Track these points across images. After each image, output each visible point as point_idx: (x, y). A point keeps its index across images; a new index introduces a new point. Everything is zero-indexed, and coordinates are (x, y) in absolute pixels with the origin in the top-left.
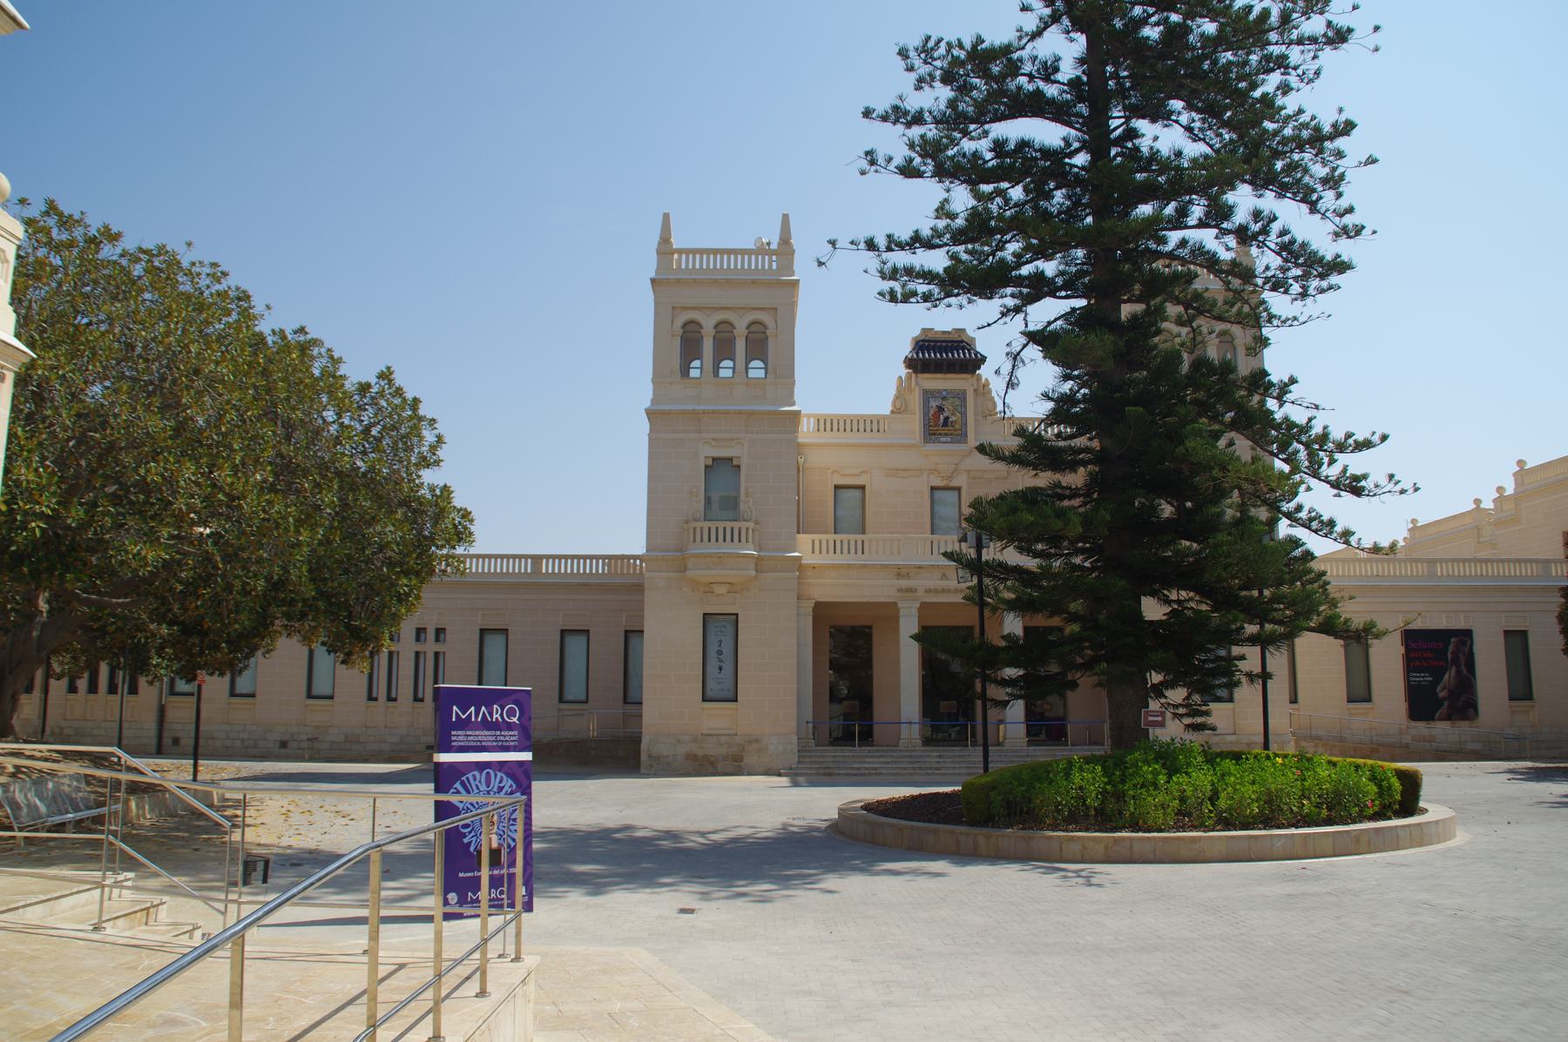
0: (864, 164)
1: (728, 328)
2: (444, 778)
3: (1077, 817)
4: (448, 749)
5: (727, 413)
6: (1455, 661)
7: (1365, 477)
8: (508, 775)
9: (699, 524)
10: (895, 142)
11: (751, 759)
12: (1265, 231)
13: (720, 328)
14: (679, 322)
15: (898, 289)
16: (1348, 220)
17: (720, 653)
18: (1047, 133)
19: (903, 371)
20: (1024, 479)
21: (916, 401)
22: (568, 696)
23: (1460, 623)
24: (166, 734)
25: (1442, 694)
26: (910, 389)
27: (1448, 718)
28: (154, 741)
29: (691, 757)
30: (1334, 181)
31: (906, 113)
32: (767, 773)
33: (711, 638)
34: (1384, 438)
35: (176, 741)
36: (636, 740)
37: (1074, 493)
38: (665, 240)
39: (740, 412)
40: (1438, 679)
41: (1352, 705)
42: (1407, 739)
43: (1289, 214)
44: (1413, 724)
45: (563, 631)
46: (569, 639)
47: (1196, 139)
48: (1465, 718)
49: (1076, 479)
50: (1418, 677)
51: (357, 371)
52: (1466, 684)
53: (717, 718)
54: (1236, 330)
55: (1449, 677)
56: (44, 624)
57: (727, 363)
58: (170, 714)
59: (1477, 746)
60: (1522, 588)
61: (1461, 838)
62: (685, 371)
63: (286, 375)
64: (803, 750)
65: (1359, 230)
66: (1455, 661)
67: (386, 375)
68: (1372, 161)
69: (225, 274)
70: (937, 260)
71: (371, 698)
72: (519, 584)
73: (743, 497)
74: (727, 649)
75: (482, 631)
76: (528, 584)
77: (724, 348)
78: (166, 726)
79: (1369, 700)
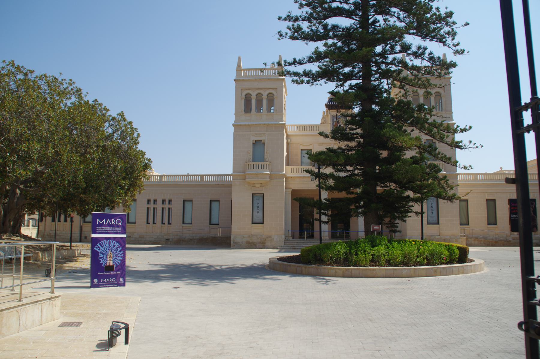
0: (278, 36)
1: (417, 94)
2: (94, 242)
3: (337, 262)
4: (95, 232)
5: (260, 125)
7: (461, 142)
8: (117, 242)
10: (284, 26)
11: (267, 244)
12: (423, 53)
14: (244, 94)
15: (299, 81)
16: (458, 48)
17: (258, 207)
18: (344, 22)
19: (325, 109)
20: (334, 144)
21: (329, 120)
22: (213, 222)
24: (83, 236)
26: (327, 115)
28: (79, 238)
29: (248, 243)
30: (453, 34)
31: (292, 17)
32: (274, 248)
33: (255, 202)
34: (470, 128)
35: (86, 238)
36: (229, 238)
37: (352, 149)
38: (239, 66)
39: (264, 124)
42: (510, 238)
43: (435, 48)
44: (512, 233)
45: (184, 201)
47: (401, 21)
49: (353, 144)
50: (514, 216)
51: (113, 113)
53: (257, 229)
54: (419, 89)
56: (18, 197)
58: (84, 229)
61: (486, 270)
63: (89, 115)
64: (286, 240)
65: (463, 51)
67: (122, 114)
68: (467, 24)
69: (74, 83)
70: (314, 67)
71: (148, 223)
72: (196, 185)
73: (265, 154)
75: (184, 201)
78: (83, 233)
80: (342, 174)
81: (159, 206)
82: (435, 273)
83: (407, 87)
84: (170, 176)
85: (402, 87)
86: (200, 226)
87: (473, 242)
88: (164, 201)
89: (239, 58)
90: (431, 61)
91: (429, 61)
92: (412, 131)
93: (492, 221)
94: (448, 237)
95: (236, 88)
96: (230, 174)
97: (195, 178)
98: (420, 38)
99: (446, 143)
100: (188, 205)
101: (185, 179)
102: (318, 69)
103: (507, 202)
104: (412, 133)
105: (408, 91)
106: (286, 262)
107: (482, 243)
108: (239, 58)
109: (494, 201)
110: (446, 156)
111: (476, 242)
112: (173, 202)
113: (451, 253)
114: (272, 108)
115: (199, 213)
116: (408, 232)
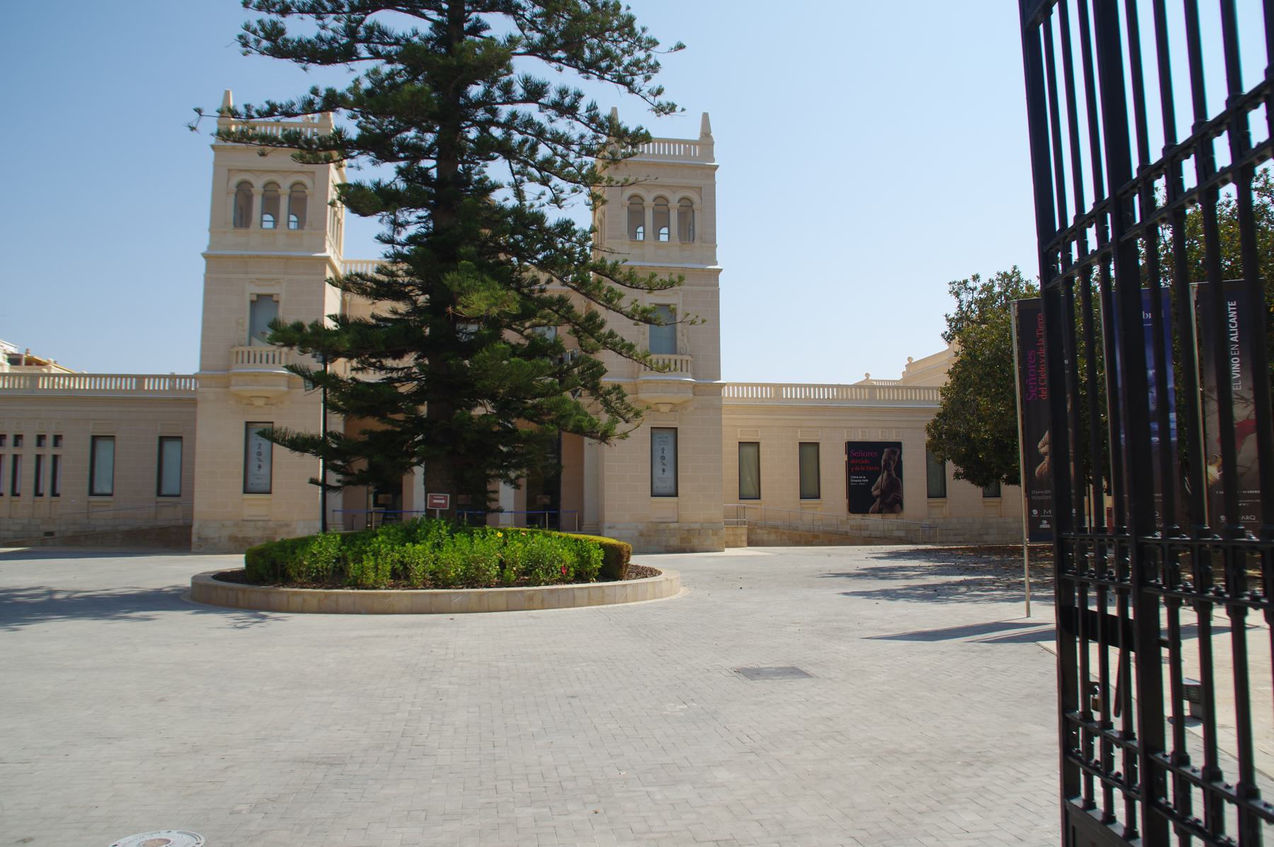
1: (664, 202)
3: (318, 580)
5: (269, 257)
9: (242, 349)
13: (295, 188)
17: (259, 454)
23: (892, 437)
27: (880, 511)
33: (656, 446)
39: (280, 257)
40: (873, 480)
41: (931, 500)
42: (847, 528)
43: (601, 94)
44: (853, 516)
45: (162, 439)
46: (100, 444)
48: (892, 512)
50: (856, 479)
55: (882, 479)
59: (902, 534)
62: (633, 234)
65: (672, 108)
68: (680, 47)
74: (669, 454)
76: (132, 399)
77: (662, 219)
79: (819, 497)
80: (372, 377)
81: (29, 451)
82: (528, 604)
83: (555, 181)
84: (101, 376)
85: (545, 182)
86: (132, 497)
87: (765, 537)
88: (40, 439)
89: (705, 116)
90: (593, 126)
91: (587, 125)
92: (549, 281)
93: (810, 490)
94: (697, 526)
95: (216, 166)
96: (191, 373)
97: (758, 393)
98: (576, 71)
100: (104, 449)
101: (86, 385)
102: (358, 131)
104: (548, 287)
105: (562, 192)
106: (237, 582)
107: (785, 537)
108: (705, 116)
109: (817, 444)
110: (623, 340)
111: (773, 537)
112: (64, 442)
113: (582, 557)
114: (640, 229)
115: (130, 465)
116: (606, 513)
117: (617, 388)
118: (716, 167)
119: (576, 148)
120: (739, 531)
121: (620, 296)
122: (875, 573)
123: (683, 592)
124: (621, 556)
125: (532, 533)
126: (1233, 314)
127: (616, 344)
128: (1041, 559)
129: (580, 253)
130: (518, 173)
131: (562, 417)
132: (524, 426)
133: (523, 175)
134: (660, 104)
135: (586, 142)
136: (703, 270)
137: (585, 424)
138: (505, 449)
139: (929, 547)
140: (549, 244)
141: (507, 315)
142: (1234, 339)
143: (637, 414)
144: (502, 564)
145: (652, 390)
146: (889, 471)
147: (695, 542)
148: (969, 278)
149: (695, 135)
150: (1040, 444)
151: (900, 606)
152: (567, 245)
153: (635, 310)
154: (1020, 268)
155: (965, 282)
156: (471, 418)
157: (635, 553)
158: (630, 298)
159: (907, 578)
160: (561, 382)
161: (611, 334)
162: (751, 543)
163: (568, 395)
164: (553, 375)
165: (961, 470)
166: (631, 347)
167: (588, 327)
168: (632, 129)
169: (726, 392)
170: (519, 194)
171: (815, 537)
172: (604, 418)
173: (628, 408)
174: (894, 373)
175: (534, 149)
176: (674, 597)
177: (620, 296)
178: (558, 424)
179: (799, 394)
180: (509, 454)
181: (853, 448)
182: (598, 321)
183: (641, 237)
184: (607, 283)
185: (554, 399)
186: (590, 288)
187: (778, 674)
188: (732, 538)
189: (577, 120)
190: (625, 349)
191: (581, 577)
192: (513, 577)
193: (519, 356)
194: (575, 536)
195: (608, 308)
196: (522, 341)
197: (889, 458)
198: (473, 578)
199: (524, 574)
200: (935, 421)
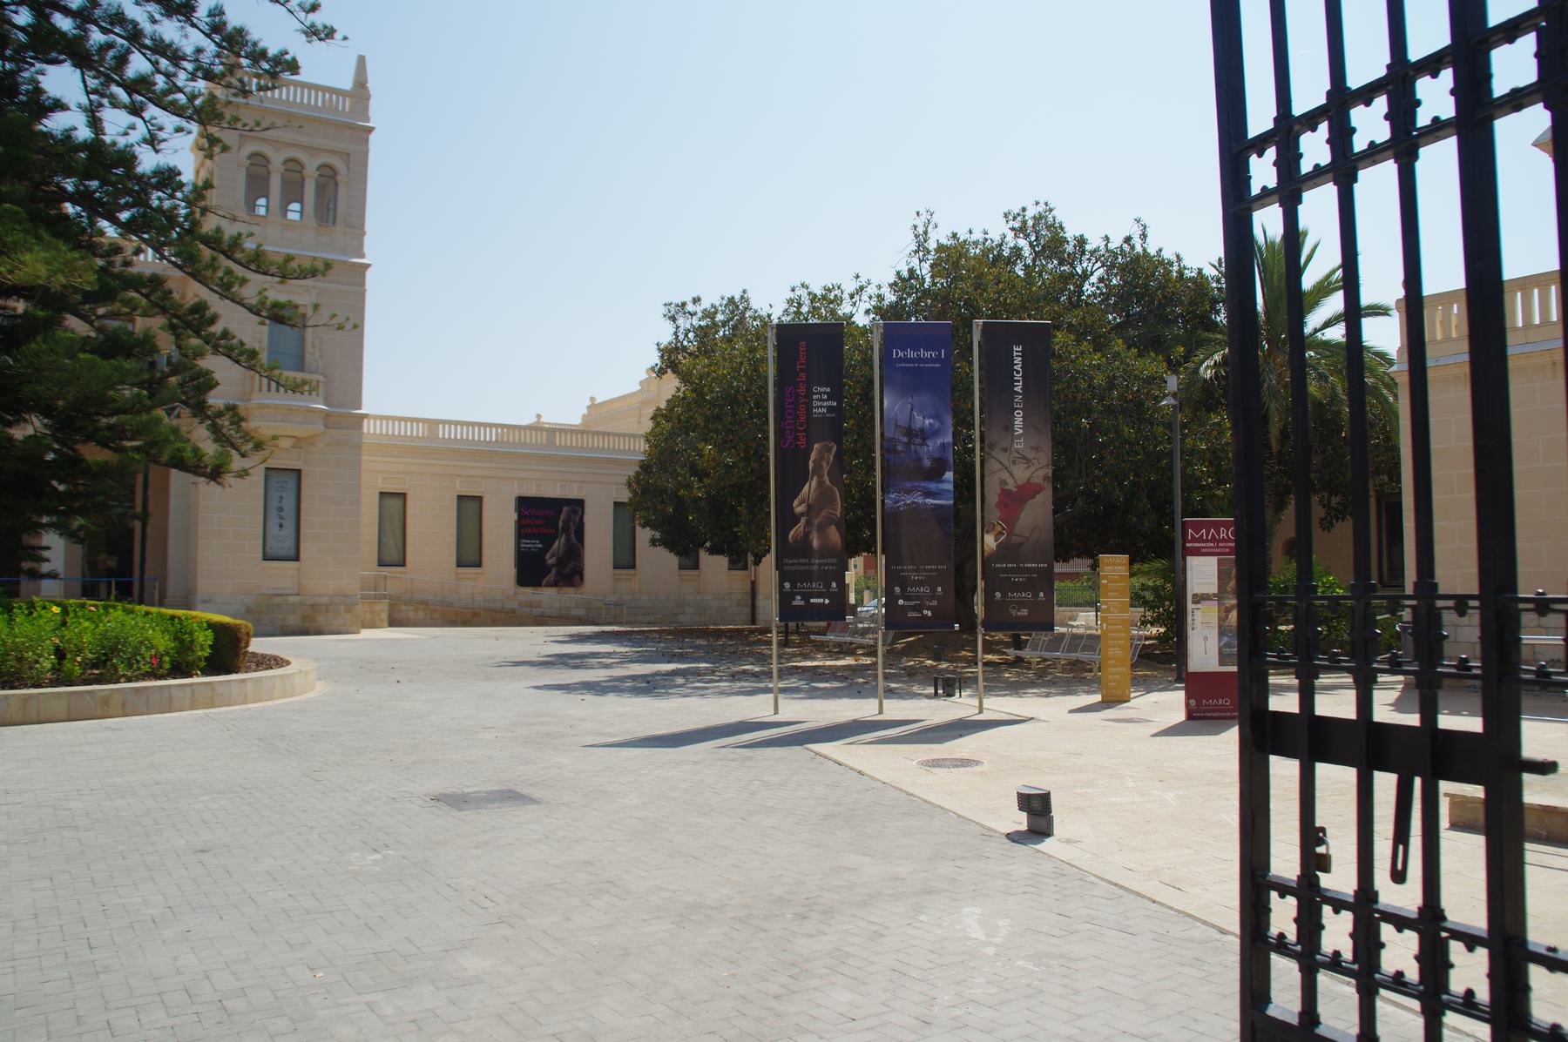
1: (297, 167)
6: (566, 529)
23: (572, 493)
25: (551, 561)
27: (555, 584)
28: (747, 610)
42: (515, 605)
48: (571, 585)
50: (529, 544)
52: (575, 552)
53: (280, 576)
55: (559, 544)
57: (296, 206)
59: (581, 612)
60: (579, 459)
62: (252, 207)
65: (330, 33)
66: (566, 529)
74: (289, 504)
77: (293, 191)
79: (480, 565)
82: (102, 710)
83: (152, 111)
85: (136, 110)
87: (411, 615)
89: (361, 60)
90: (217, 38)
92: (138, 252)
93: (469, 555)
94: (325, 600)
99: (240, 303)
103: (512, 505)
105: (161, 129)
109: (479, 499)
110: (242, 344)
111: (421, 615)
113: (182, 642)
117: (232, 408)
118: (371, 130)
119: (189, 66)
120: (377, 608)
121: (244, 282)
122: (563, 661)
123: (320, 689)
124: (238, 640)
125: (106, 608)
126: (1018, 360)
127: (231, 349)
128: (754, 643)
129: (186, 217)
130: (95, 92)
131: (153, 443)
132: (94, 454)
133: (103, 95)
134: (313, 25)
135: (205, 59)
136: (345, 263)
137: (188, 454)
138: (61, 488)
139: (616, 628)
140: (141, 200)
141: (77, 290)
142: (1018, 389)
143: (258, 446)
144: (60, 654)
145: (270, 412)
146: (568, 535)
147: (322, 620)
148: (689, 300)
149: (347, 84)
150: (796, 503)
151: (613, 705)
152: (167, 204)
153: (263, 303)
154: (749, 294)
155: (684, 304)
156: (11, 439)
157: (257, 635)
158: (255, 286)
159: (606, 666)
160: (151, 396)
161: (226, 334)
162: (394, 622)
163: (160, 412)
164: (140, 385)
165: (658, 535)
166: (253, 354)
167: (195, 320)
168: (272, 52)
169: (368, 427)
170: (95, 123)
171: (476, 615)
172: (209, 448)
173: (247, 437)
174: (570, 414)
175: (122, 60)
176: (310, 695)
177: (244, 282)
178: (148, 454)
179: (458, 433)
180: (68, 495)
181: (524, 504)
182: (208, 314)
183: (262, 211)
184: (225, 262)
185: (145, 417)
186: (199, 266)
187: (492, 801)
188: (368, 616)
189: (194, 25)
190: (245, 357)
191: (180, 669)
192: (78, 670)
193: (91, 352)
194: (170, 612)
195: (223, 296)
196: (93, 334)
197: (569, 519)
198: (12, 674)
199: (95, 666)
200: (637, 473)
